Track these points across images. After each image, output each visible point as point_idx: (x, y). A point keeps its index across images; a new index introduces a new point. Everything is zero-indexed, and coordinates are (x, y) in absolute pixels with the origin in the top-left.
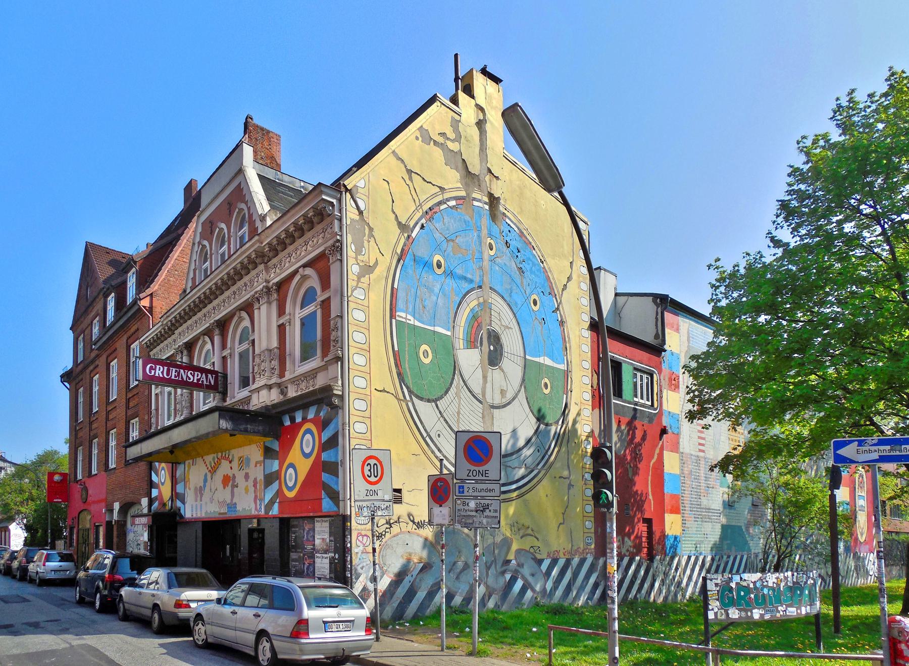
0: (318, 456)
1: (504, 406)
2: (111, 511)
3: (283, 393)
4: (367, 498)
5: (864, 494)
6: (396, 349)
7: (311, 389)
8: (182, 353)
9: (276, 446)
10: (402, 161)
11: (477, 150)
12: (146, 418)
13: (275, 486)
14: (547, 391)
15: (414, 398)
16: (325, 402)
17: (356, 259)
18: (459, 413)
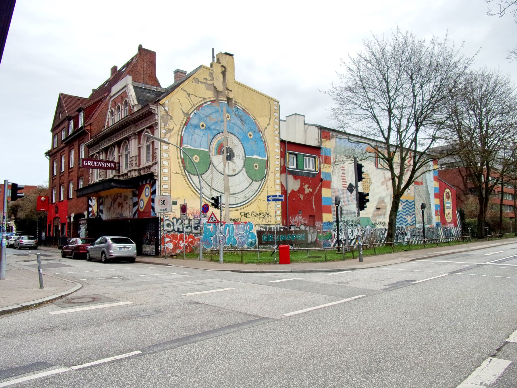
0: (150, 197)
1: (235, 175)
2: (70, 218)
3: (140, 173)
5: (450, 201)
6: (182, 157)
9: (137, 192)
10: (185, 91)
11: (222, 82)
13: (136, 208)
14: (257, 169)
16: (149, 178)
18: (212, 179)
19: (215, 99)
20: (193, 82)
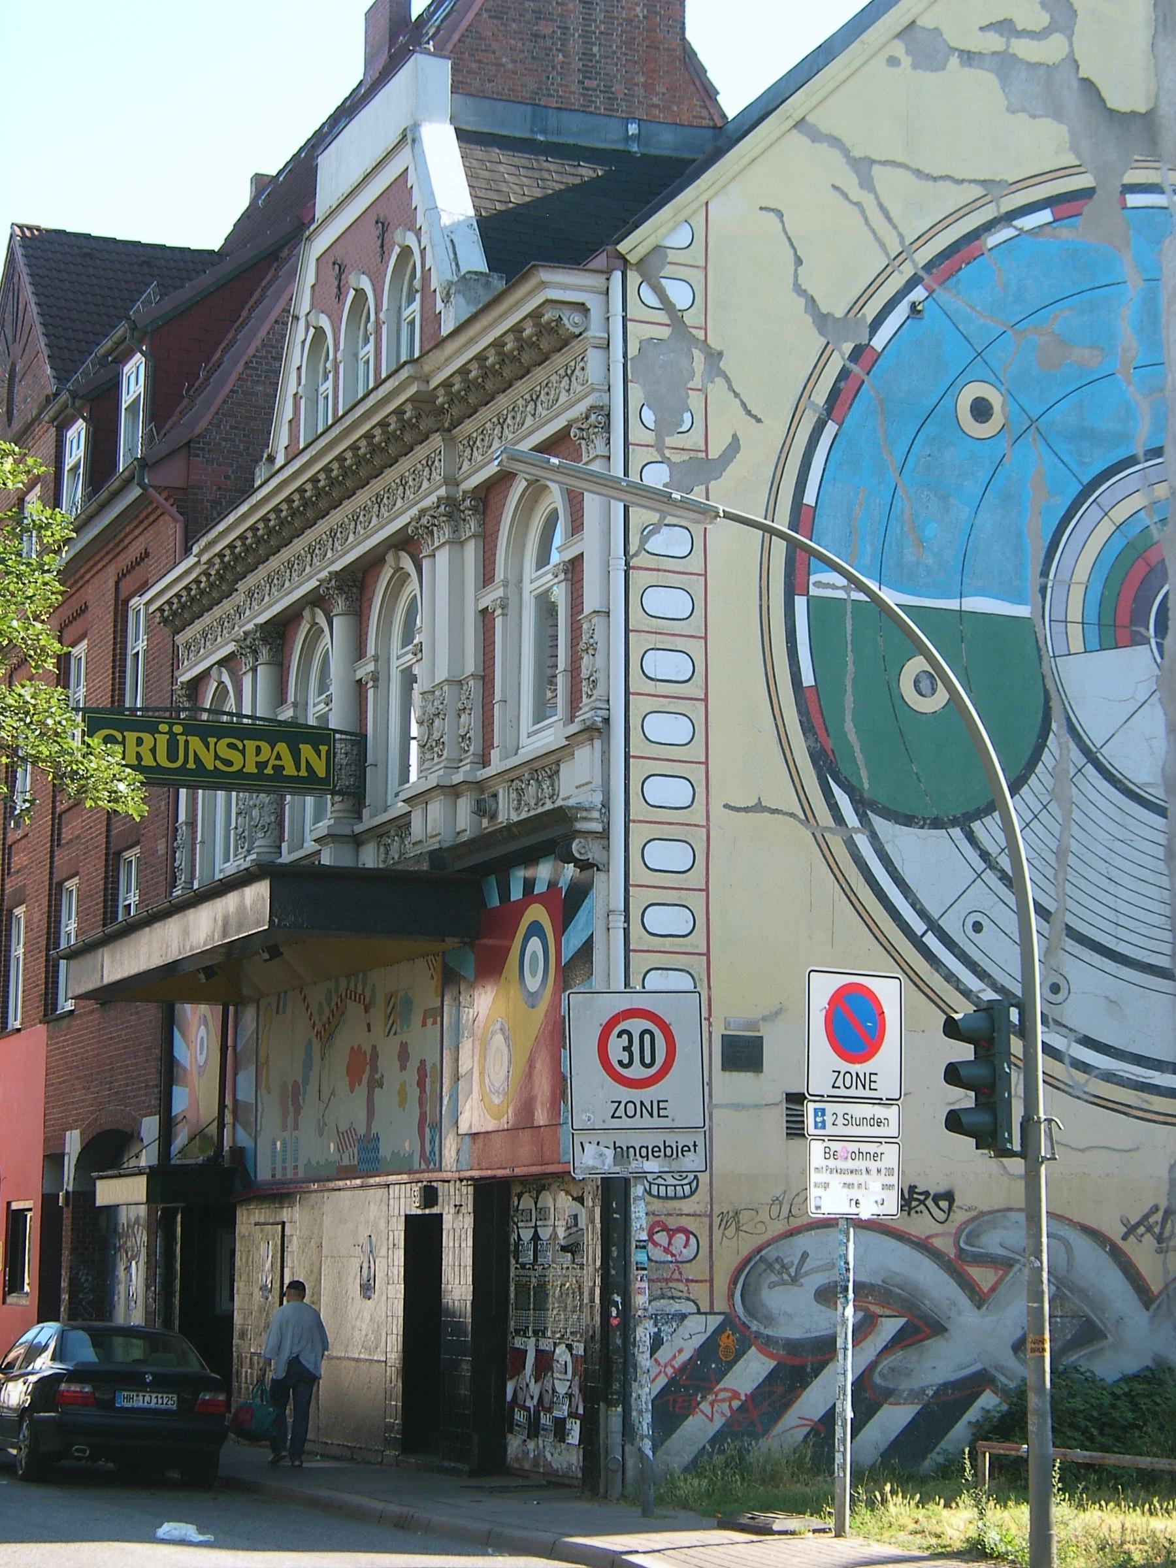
4: (616, 1123)
6: (808, 679)
7: (549, 806)
8: (255, 652)
12: (161, 847)
15: (877, 821)
17: (659, 446)
19: (1084, 181)
20: (893, 61)
